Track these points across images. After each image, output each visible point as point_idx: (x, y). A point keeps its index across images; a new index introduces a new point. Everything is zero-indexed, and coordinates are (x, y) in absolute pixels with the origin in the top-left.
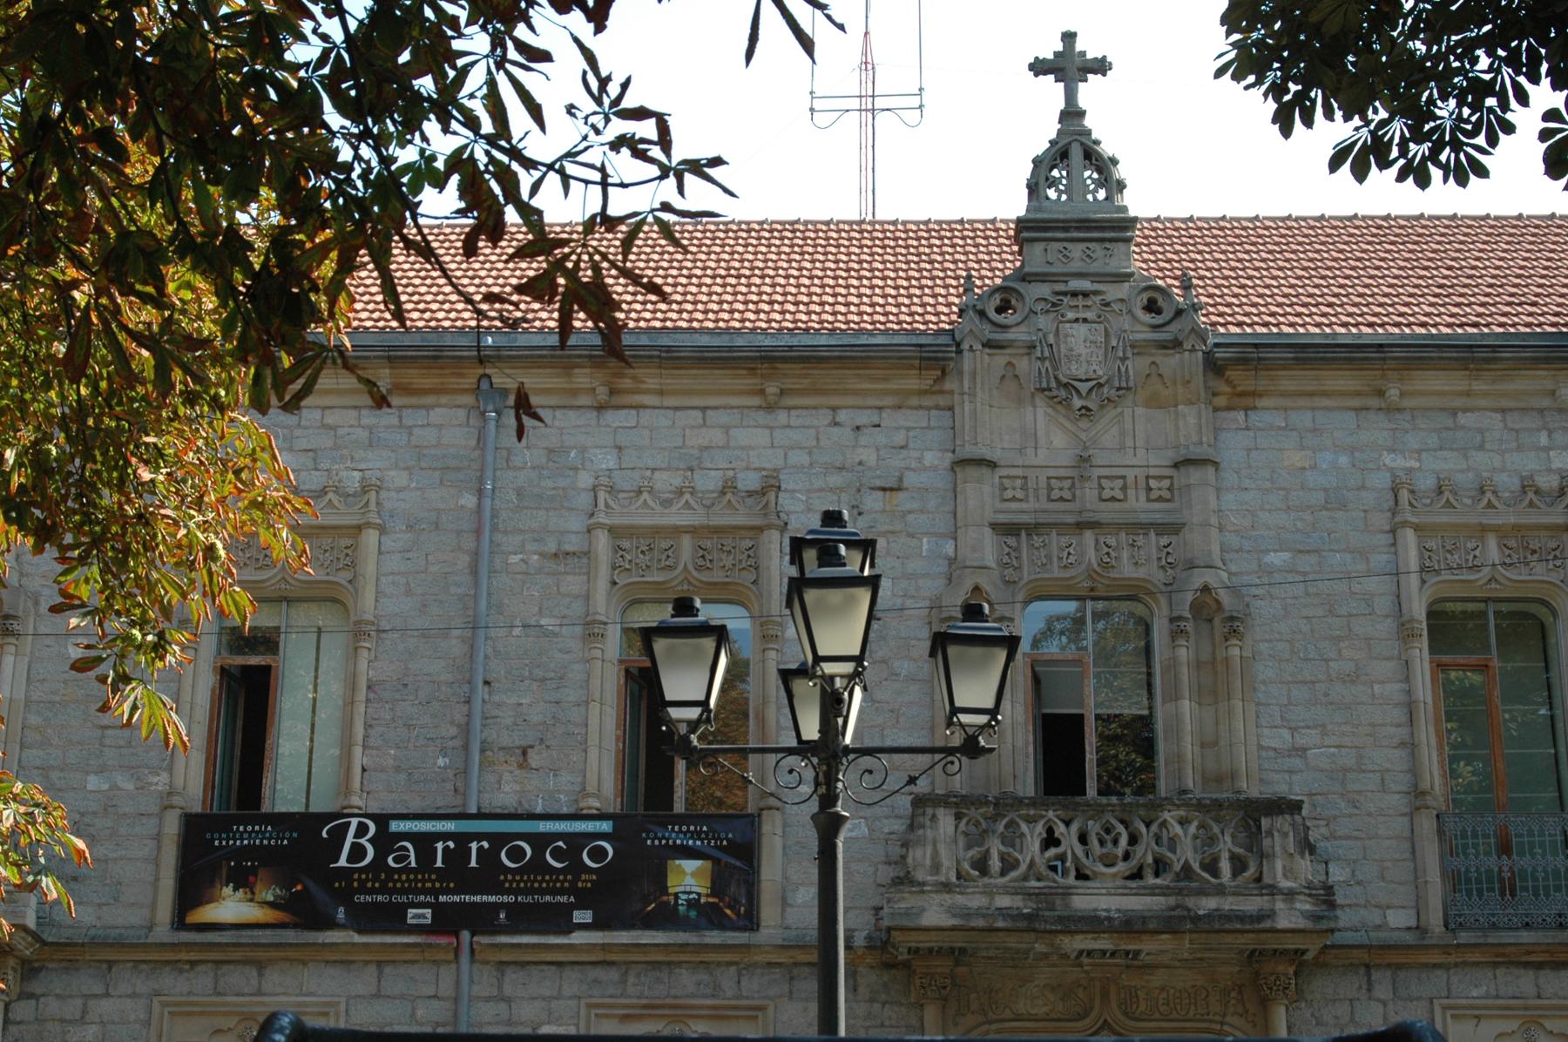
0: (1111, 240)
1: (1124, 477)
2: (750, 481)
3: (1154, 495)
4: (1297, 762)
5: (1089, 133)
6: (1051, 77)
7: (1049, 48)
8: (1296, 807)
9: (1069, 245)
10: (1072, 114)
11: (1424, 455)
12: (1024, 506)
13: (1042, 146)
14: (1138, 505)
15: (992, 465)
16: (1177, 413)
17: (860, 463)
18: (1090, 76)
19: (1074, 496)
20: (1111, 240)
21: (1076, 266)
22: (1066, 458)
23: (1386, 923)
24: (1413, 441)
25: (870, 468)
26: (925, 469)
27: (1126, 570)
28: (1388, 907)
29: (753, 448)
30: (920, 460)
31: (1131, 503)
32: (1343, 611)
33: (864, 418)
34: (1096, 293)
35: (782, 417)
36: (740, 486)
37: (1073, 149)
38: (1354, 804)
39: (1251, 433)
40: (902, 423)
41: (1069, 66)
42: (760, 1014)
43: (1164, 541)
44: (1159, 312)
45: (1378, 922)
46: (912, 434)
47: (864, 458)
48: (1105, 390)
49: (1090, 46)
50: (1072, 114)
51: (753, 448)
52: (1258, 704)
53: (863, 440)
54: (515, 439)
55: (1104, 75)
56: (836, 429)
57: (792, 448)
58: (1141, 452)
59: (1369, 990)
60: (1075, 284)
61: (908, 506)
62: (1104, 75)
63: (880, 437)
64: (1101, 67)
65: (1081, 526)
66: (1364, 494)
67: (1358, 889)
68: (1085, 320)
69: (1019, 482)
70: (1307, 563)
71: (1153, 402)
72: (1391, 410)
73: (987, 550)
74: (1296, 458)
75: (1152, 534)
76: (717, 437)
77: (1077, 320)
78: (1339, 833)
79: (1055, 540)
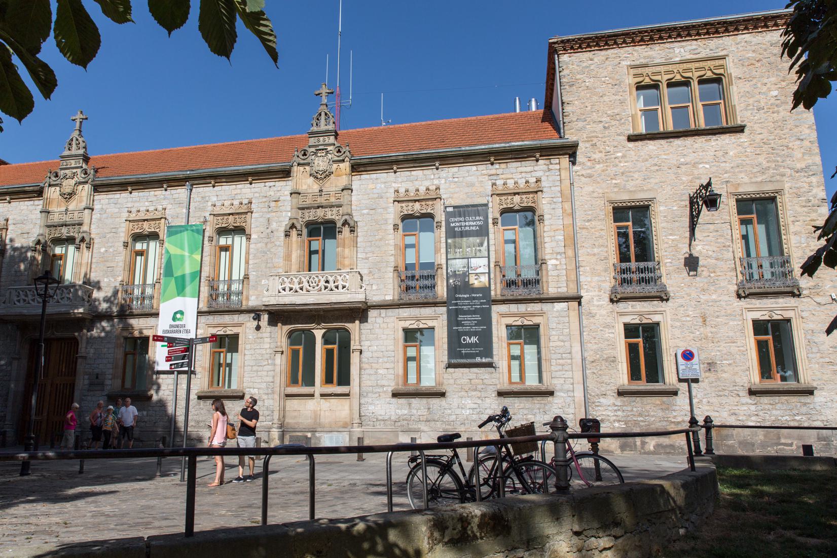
2: (245, 201)
14: (333, 200)
21: (321, 142)
54: (743, 138)
60: (321, 147)
63: (275, 189)
65: (318, 207)
74: (371, 186)
76: (239, 191)
79: (313, 211)
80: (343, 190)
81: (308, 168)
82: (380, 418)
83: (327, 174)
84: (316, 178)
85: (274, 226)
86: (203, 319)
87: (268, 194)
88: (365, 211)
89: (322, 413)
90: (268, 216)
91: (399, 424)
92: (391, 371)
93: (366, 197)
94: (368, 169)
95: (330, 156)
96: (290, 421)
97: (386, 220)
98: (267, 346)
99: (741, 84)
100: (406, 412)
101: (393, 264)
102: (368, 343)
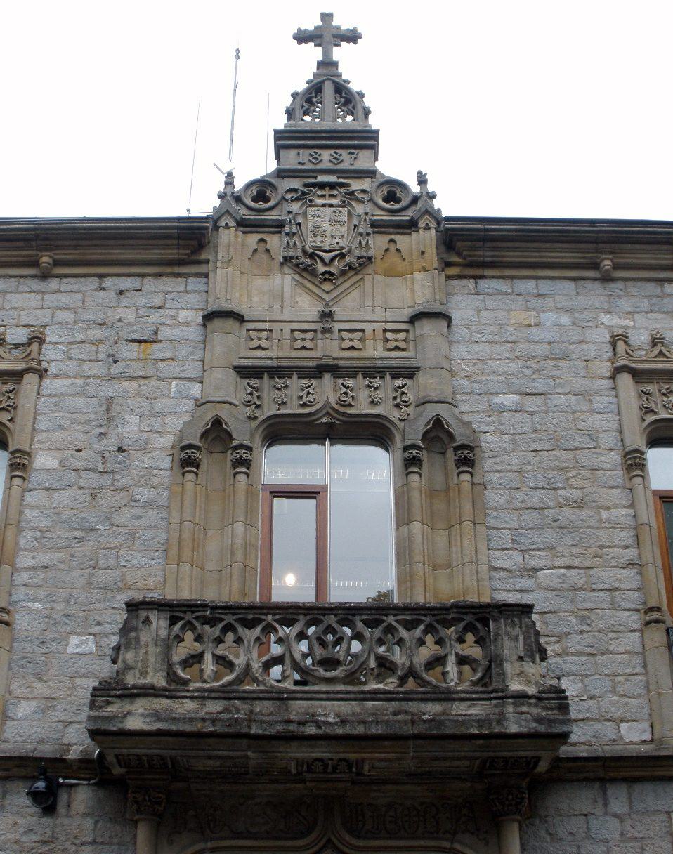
0: (355, 147)
1: (363, 331)
3: (392, 345)
4: (530, 583)
5: (340, 75)
6: (312, 44)
7: (311, 23)
8: (527, 609)
9: (319, 151)
10: (327, 64)
11: (637, 316)
12: (267, 354)
13: (302, 87)
14: (375, 352)
15: (240, 319)
16: (413, 279)
17: (120, 320)
18: (343, 44)
19: (316, 345)
20: (355, 147)
21: (326, 165)
22: (313, 314)
23: (621, 738)
24: (625, 304)
25: (128, 324)
26: (180, 324)
27: (362, 407)
28: (622, 721)
29: (23, 309)
30: (174, 318)
32: (571, 445)
33: (127, 283)
34: (342, 185)
35: (53, 284)
36: (8, 339)
37: (328, 88)
38: (584, 620)
39: (481, 297)
40: (161, 288)
41: (326, 35)
43: (399, 382)
44: (398, 201)
45: (613, 736)
46: (168, 296)
47: (123, 316)
48: (347, 259)
49: (343, 22)
50: (327, 64)
51: (23, 309)
52: (489, 528)
53: (125, 302)
55: (355, 42)
56: (101, 293)
57: (59, 309)
58: (379, 311)
59: (606, 805)
61: (161, 355)
62: (355, 42)
63: (140, 300)
64: (352, 37)
66: (585, 346)
67: (591, 702)
68: (331, 206)
69: (265, 334)
70: (532, 404)
71: (391, 272)
72: (606, 279)
73: (231, 389)
75: (388, 377)
77: (324, 206)
79: (295, 383)
80: (413, 320)
85: (131, 427)
87: (113, 315)
88: (509, 400)
93: (505, 350)
94: (511, 256)
97: (593, 435)
99: (23, 589)
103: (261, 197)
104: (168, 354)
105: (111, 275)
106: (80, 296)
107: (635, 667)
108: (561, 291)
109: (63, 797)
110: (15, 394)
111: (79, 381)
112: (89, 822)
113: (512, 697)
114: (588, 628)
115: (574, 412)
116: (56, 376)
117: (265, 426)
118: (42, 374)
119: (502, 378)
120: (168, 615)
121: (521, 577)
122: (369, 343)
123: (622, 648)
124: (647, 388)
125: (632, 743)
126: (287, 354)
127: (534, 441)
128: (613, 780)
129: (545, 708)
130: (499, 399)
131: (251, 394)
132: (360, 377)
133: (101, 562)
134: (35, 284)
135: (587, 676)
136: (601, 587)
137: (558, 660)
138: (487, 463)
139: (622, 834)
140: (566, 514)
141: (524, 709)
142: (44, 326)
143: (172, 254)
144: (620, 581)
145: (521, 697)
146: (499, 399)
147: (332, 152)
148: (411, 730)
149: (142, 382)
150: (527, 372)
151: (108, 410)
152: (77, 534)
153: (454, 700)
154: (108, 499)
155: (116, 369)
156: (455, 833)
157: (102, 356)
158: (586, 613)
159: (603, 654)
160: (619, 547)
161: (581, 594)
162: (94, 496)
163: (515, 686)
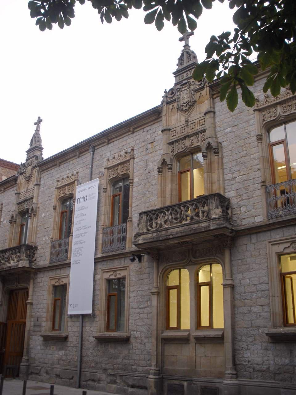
2: (129, 150)
3: (201, 124)
4: (234, 182)
10: (187, 46)
12: (175, 137)
21: (185, 78)
23: (255, 221)
27: (195, 144)
28: (256, 216)
31: (197, 128)
34: (188, 82)
38: (246, 189)
42: (127, 268)
45: (254, 221)
53: (148, 133)
57: (136, 140)
59: (251, 241)
63: (151, 132)
70: (234, 129)
78: (244, 199)
79: (181, 142)
80: (206, 114)
81: (175, 105)
82: (258, 368)
83: (191, 105)
84: (182, 110)
86: (100, 266)
89: (198, 359)
90: (146, 158)
91: (280, 377)
92: (266, 309)
95: (192, 87)
96: (170, 368)
97: (249, 133)
98: (146, 288)
99: (134, 212)
100: (287, 361)
101: (260, 180)
102: (240, 276)
103: (173, 93)
104: (157, 144)
105: (145, 127)
106: (140, 135)
107: (259, 200)
108: (75, 161)
109: (142, 258)
110: (276, 111)
111: (141, 158)
112: (147, 263)
113: (212, 219)
114: (248, 191)
115: (245, 128)
116: (137, 158)
117: (265, 126)
118: (134, 158)
119: (227, 124)
120: (146, 215)
121: (232, 181)
122: (196, 125)
123: (256, 195)
124: (264, 113)
125: (258, 222)
126: (200, 127)
127: (235, 140)
128: (253, 233)
129: (220, 221)
130: (226, 131)
131: (284, 109)
132: (194, 136)
133: (147, 201)
134: (132, 136)
135: (247, 205)
136: (251, 179)
137: (241, 202)
138: (226, 151)
139: (255, 248)
140: (243, 160)
141: (215, 222)
142: (134, 146)
143: (154, 118)
144: (256, 175)
145: (215, 219)
146: (226, 131)
147: (185, 73)
148: (190, 233)
149: (152, 153)
150: (233, 119)
151: (146, 163)
152: (142, 196)
153: (200, 223)
154: (148, 185)
155: (148, 151)
156: (215, 254)
157: (145, 149)
158: (247, 187)
159: (251, 198)
160: (256, 165)
161: (246, 182)
162: (145, 185)
163: (213, 216)
